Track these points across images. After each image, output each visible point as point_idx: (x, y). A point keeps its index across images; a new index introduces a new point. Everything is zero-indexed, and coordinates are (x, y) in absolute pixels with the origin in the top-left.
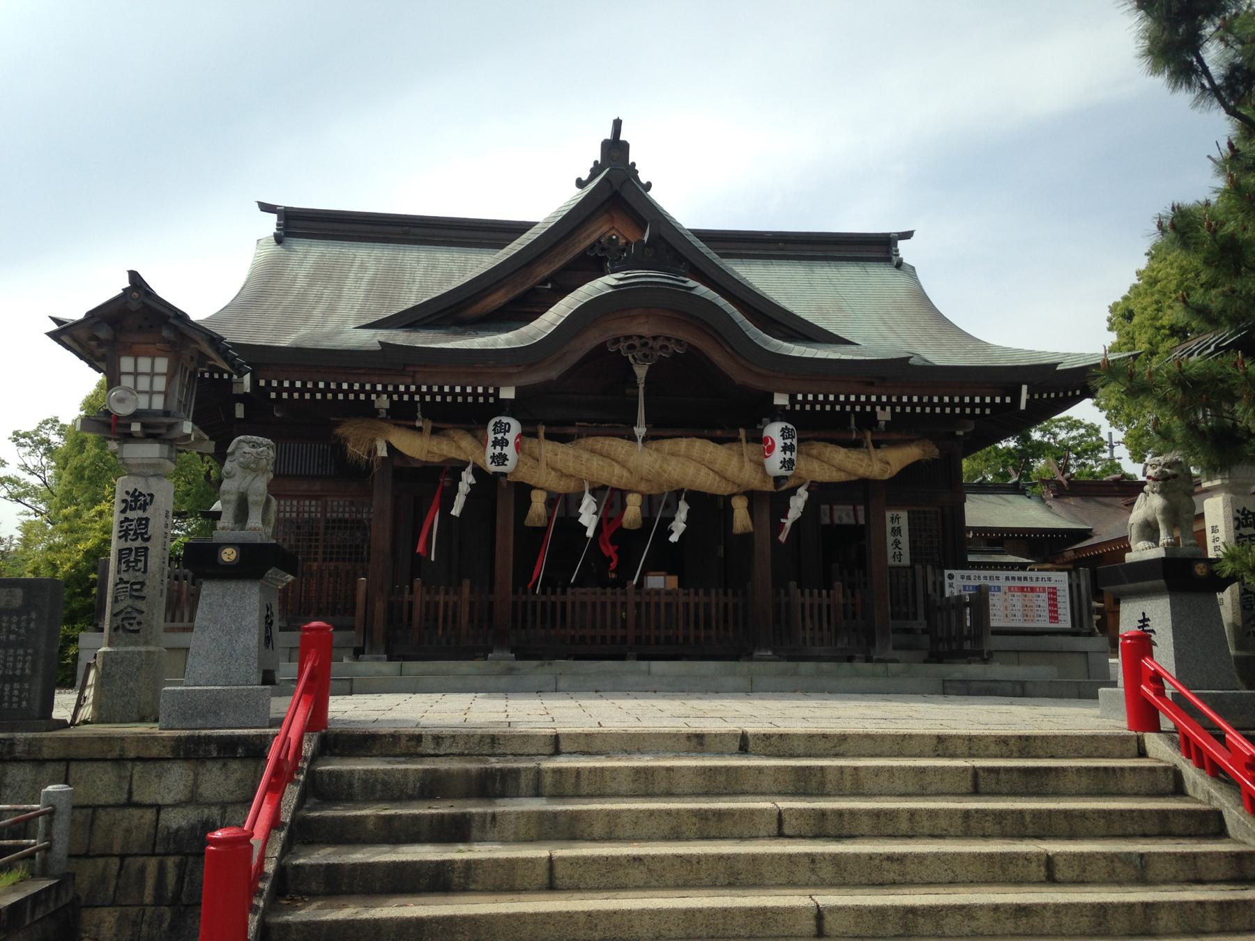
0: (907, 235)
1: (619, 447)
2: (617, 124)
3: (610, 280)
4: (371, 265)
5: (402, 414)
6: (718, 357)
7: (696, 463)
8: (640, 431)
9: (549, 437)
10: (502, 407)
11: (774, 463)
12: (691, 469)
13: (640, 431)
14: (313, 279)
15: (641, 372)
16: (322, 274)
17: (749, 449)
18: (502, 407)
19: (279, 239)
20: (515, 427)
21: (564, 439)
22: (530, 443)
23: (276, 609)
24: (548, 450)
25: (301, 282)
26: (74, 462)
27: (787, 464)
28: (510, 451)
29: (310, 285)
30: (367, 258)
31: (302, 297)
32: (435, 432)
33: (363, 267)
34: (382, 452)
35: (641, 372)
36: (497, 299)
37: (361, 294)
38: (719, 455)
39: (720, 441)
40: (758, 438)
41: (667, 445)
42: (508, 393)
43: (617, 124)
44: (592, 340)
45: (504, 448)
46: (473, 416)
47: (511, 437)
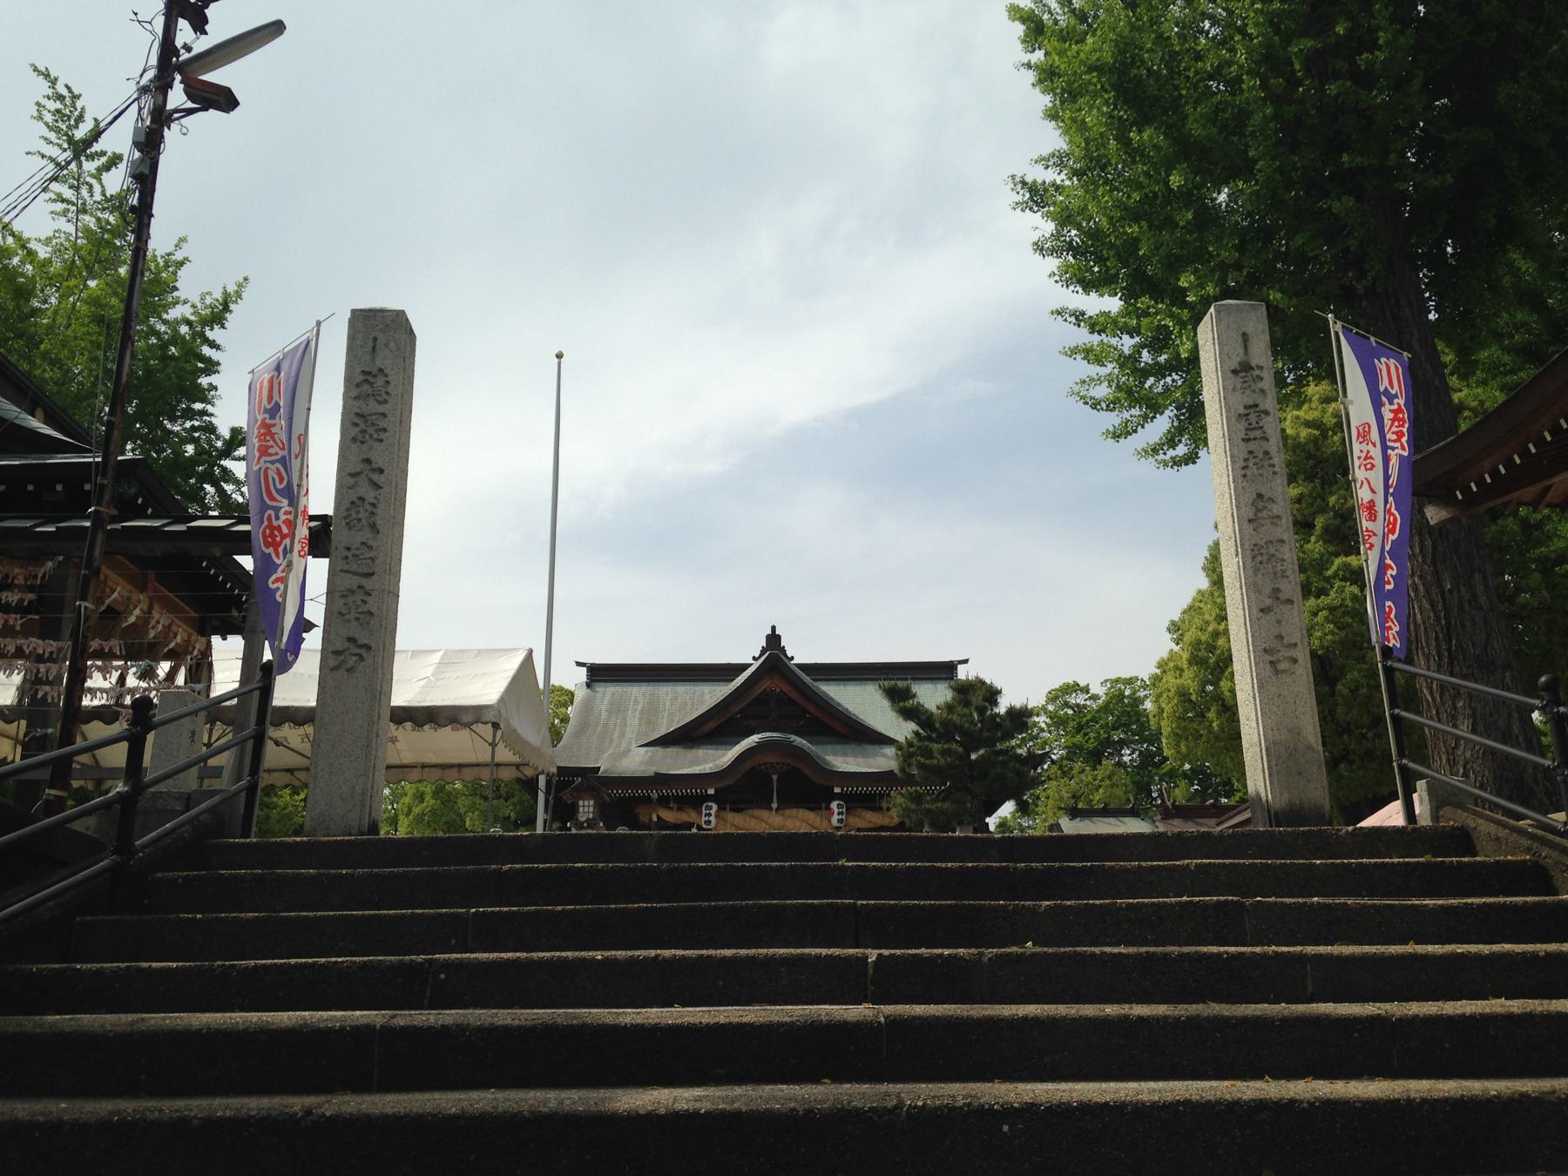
0: (966, 661)
1: (764, 814)
2: (774, 628)
3: (754, 739)
4: (641, 699)
5: (664, 802)
6: (807, 771)
7: (799, 821)
8: (775, 805)
9: (732, 810)
10: (708, 798)
11: (835, 819)
12: (798, 824)
13: (775, 805)
14: (610, 711)
15: (775, 777)
16: (617, 708)
17: (825, 813)
18: (708, 798)
19: (588, 685)
20: (715, 807)
21: (738, 811)
22: (723, 814)
23: (1231, 567)
24: (730, 816)
25: (604, 715)
26: (416, 810)
27: (840, 821)
28: (712, 818)
29: (609, 717)
30: (638, 693)
31: (606, 725)
32: (679, 809)
33: (636, 702)
34: (655, 818)
35: (775, 777)
36: (711, 726)
37: (636, 722)
38: (810, 816)
39: (812, 809)
40: (828, 808)
41: (787, 812)
42: (711, 791)
43: (774, 628)
44: (747, 766)
45: (711, 819)
46: (696, 802)
47: (713, 812)
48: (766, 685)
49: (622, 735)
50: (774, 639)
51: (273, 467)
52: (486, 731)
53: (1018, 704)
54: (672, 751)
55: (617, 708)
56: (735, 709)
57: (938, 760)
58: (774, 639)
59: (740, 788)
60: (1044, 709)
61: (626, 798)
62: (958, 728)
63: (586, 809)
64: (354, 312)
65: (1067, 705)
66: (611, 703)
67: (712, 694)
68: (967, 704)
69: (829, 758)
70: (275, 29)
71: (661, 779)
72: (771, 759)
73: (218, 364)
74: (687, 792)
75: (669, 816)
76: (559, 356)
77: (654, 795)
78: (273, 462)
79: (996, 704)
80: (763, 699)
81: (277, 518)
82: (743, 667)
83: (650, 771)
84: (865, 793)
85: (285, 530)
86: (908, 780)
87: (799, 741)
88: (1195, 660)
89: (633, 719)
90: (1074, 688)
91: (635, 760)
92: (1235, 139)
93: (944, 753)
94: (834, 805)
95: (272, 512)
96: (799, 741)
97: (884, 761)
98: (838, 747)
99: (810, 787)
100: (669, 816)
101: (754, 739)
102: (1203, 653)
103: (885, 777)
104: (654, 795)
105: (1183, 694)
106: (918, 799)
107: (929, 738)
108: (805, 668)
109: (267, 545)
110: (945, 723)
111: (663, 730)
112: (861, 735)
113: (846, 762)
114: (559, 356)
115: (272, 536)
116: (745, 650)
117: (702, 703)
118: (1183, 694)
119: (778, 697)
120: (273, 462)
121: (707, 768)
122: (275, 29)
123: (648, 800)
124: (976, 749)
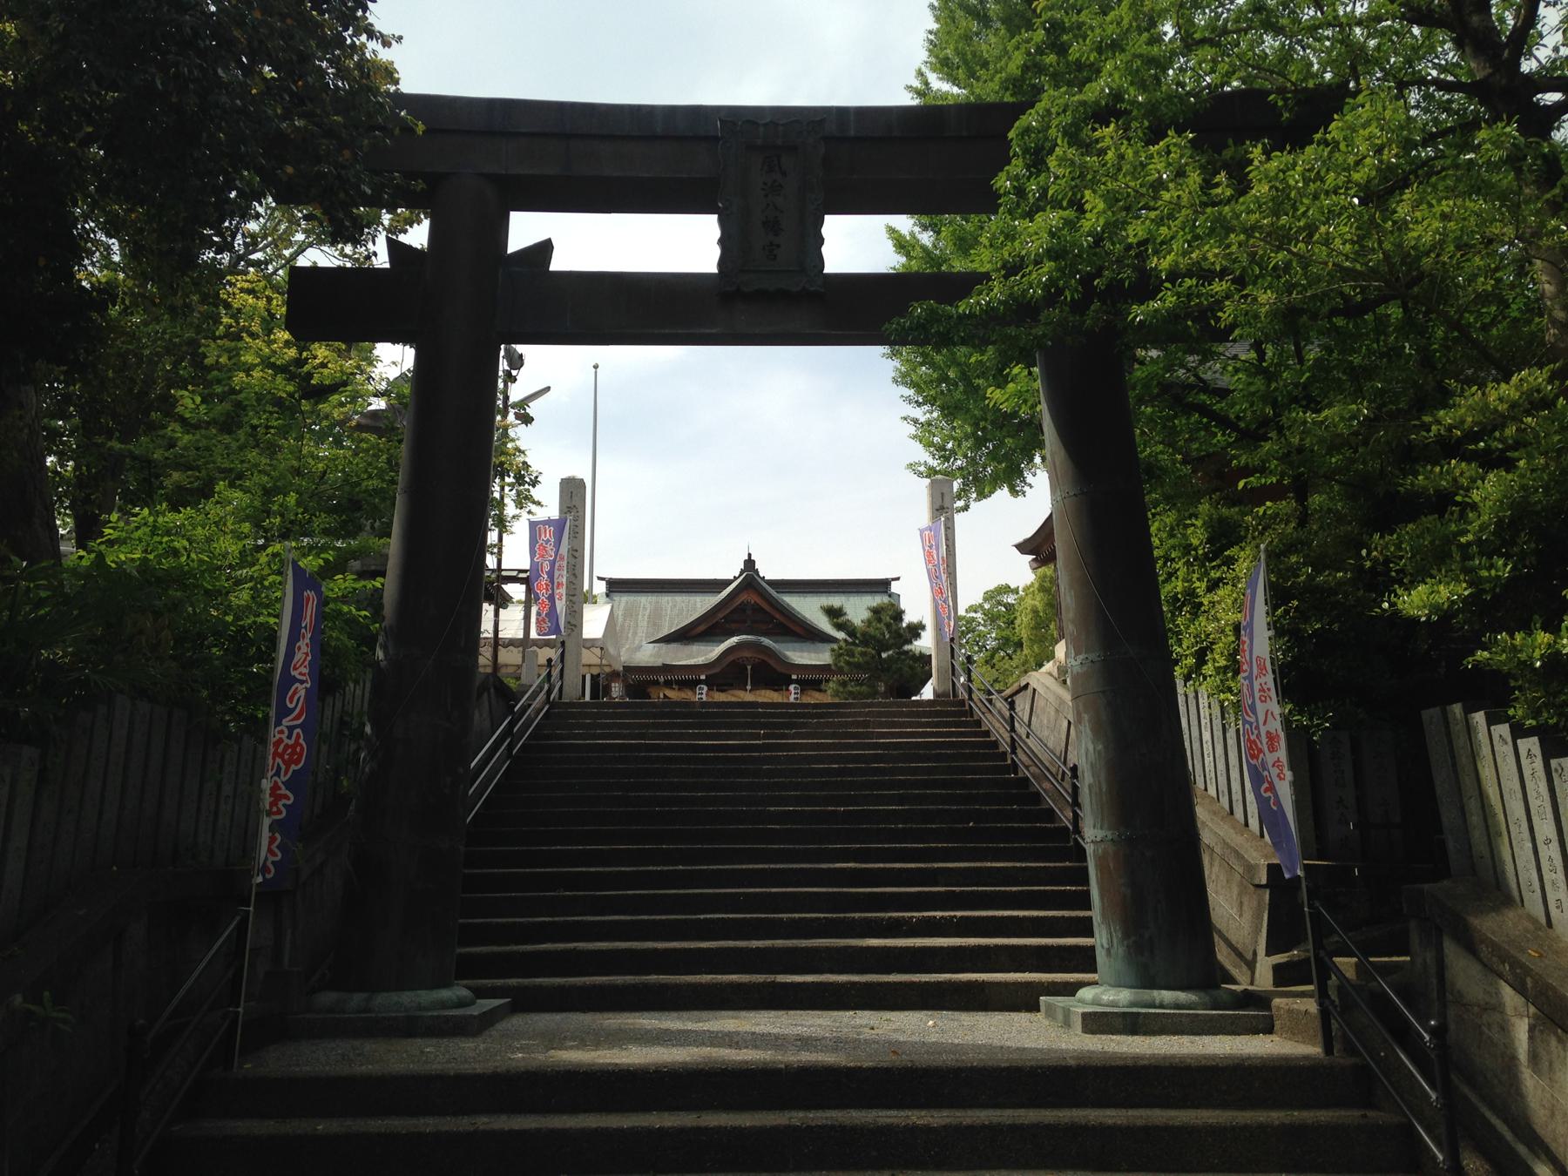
3: (734, 640)
5: (668, 684)
6: (772, 662)
7: (768, 696)
10: (700, 682)
14: (625, 616)
16: (630, 613)
18: (700, 682)
30: (645, 601)
36: (702, 628)
44: (731, 658)
46: (692, 684)
48: (743, 597)
49: (635, 633)
50: (750, 563)
52: (598, 651)
53: (915, 620)
54: (673, 646)
55: (630, 613)
56: (721, 615)
57: (858, 659)
58: (750, 563)
59: (725, 674)
60: (981, 606)
61: (640, 681)
62: (874, 637)
63: (616, 690)
65: (999, 603)
66: (625, 610)
67: (703, 604)
68: (880, 620)
69: (789, 653)
70: (548, 389)
71: (666, 668)
72: (747, 654)
75: (673, 694)
76: (596, 367)
77: (662, 679)
79: (901, 620)
80: (742, 608)
82: (727, 583)
83: (659, 662)
84: (812, 679)
86: (840, 671)
87: (766, 641)
88: (1042, 589)
89: (643, 623)
90: (1005, 589)
91: (647, 654)
93: (863, 654)
94: (792, 687)
96: (766, 641)
97: (816, 656)
98: (797, 645)
99: (774, 674)
100: (673, 694)
102: (1047, 584)
103: (824, 668)
104: (662, 679)
105: (1035, 611)
106: (844, 684)
107: (853, 644)
108: (773, 583)
110: (864, 634)
111: (665, 632)
112: (811, 635)
113: (802, 656)
114: (596, 367)
116: (728, 569)
117: (695, 609)
118: (1035, 611)
119: (752, 605)
121: (700, 660)
122: (548, 389)
123: (656, 683)
124: (887, 650)
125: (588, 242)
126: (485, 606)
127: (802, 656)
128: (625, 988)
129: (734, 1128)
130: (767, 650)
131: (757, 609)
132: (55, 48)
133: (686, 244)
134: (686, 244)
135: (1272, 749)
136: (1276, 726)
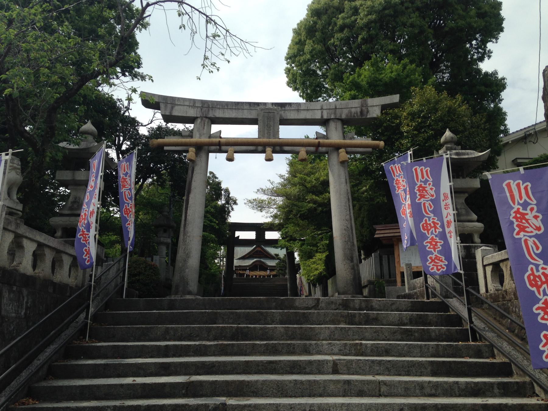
3: (255, 260)
5: (240, 270)
7: (262, 273)
46: (245, 270)
51: (428, 203)
59: (253, 268)
64: (501, 3)
71: (240, 266)
73: (145, 80)
74: (244, 268)
78: (427, 201)
80: (257, 251)
81: (429, 220)
84: (272, 269)
85: (432, 225)
92: (184, 391)
95: (427, 219)
96: (262, 260)
99: (264, 268)
101: (255, 260)
103: (275, 266)
109: (125, 214)
113: (271, 263)
115: (127, 211)
120: (427, 201)
125: (230, 132)
126: (398, 96)
127: (271, 263)
128: (213, 364)
129: (276, 356)
130: (260, 261)
131: (260, 251)
132: (127, 74)
133: (250, 132)
134: (250, 132)
135: (448, 227)
136: (451, 218)
